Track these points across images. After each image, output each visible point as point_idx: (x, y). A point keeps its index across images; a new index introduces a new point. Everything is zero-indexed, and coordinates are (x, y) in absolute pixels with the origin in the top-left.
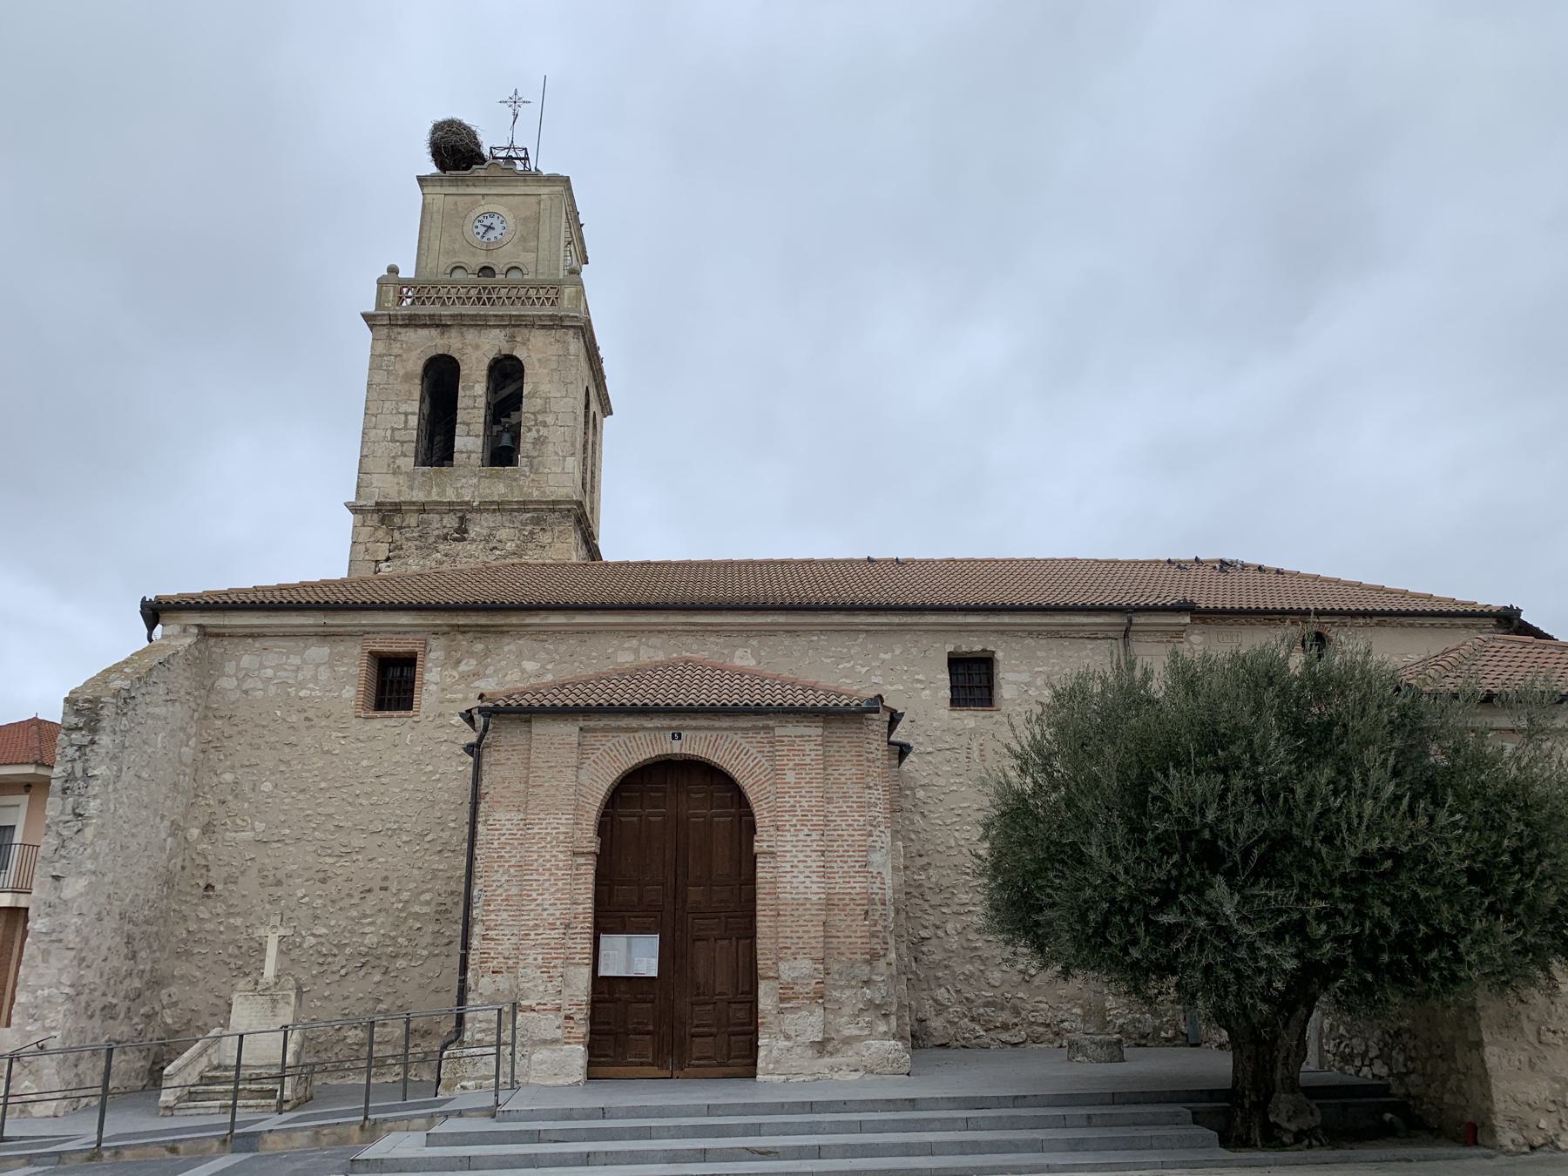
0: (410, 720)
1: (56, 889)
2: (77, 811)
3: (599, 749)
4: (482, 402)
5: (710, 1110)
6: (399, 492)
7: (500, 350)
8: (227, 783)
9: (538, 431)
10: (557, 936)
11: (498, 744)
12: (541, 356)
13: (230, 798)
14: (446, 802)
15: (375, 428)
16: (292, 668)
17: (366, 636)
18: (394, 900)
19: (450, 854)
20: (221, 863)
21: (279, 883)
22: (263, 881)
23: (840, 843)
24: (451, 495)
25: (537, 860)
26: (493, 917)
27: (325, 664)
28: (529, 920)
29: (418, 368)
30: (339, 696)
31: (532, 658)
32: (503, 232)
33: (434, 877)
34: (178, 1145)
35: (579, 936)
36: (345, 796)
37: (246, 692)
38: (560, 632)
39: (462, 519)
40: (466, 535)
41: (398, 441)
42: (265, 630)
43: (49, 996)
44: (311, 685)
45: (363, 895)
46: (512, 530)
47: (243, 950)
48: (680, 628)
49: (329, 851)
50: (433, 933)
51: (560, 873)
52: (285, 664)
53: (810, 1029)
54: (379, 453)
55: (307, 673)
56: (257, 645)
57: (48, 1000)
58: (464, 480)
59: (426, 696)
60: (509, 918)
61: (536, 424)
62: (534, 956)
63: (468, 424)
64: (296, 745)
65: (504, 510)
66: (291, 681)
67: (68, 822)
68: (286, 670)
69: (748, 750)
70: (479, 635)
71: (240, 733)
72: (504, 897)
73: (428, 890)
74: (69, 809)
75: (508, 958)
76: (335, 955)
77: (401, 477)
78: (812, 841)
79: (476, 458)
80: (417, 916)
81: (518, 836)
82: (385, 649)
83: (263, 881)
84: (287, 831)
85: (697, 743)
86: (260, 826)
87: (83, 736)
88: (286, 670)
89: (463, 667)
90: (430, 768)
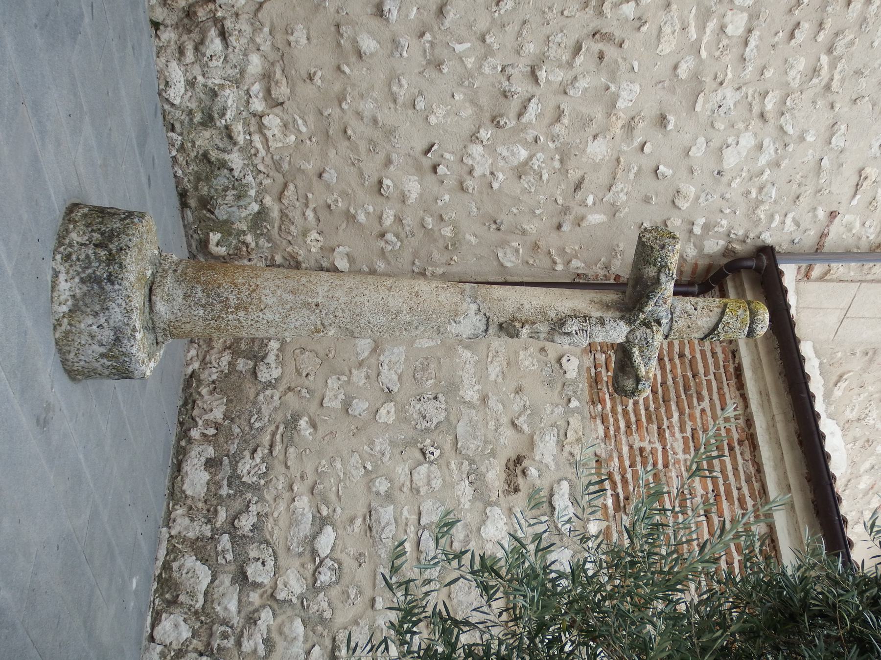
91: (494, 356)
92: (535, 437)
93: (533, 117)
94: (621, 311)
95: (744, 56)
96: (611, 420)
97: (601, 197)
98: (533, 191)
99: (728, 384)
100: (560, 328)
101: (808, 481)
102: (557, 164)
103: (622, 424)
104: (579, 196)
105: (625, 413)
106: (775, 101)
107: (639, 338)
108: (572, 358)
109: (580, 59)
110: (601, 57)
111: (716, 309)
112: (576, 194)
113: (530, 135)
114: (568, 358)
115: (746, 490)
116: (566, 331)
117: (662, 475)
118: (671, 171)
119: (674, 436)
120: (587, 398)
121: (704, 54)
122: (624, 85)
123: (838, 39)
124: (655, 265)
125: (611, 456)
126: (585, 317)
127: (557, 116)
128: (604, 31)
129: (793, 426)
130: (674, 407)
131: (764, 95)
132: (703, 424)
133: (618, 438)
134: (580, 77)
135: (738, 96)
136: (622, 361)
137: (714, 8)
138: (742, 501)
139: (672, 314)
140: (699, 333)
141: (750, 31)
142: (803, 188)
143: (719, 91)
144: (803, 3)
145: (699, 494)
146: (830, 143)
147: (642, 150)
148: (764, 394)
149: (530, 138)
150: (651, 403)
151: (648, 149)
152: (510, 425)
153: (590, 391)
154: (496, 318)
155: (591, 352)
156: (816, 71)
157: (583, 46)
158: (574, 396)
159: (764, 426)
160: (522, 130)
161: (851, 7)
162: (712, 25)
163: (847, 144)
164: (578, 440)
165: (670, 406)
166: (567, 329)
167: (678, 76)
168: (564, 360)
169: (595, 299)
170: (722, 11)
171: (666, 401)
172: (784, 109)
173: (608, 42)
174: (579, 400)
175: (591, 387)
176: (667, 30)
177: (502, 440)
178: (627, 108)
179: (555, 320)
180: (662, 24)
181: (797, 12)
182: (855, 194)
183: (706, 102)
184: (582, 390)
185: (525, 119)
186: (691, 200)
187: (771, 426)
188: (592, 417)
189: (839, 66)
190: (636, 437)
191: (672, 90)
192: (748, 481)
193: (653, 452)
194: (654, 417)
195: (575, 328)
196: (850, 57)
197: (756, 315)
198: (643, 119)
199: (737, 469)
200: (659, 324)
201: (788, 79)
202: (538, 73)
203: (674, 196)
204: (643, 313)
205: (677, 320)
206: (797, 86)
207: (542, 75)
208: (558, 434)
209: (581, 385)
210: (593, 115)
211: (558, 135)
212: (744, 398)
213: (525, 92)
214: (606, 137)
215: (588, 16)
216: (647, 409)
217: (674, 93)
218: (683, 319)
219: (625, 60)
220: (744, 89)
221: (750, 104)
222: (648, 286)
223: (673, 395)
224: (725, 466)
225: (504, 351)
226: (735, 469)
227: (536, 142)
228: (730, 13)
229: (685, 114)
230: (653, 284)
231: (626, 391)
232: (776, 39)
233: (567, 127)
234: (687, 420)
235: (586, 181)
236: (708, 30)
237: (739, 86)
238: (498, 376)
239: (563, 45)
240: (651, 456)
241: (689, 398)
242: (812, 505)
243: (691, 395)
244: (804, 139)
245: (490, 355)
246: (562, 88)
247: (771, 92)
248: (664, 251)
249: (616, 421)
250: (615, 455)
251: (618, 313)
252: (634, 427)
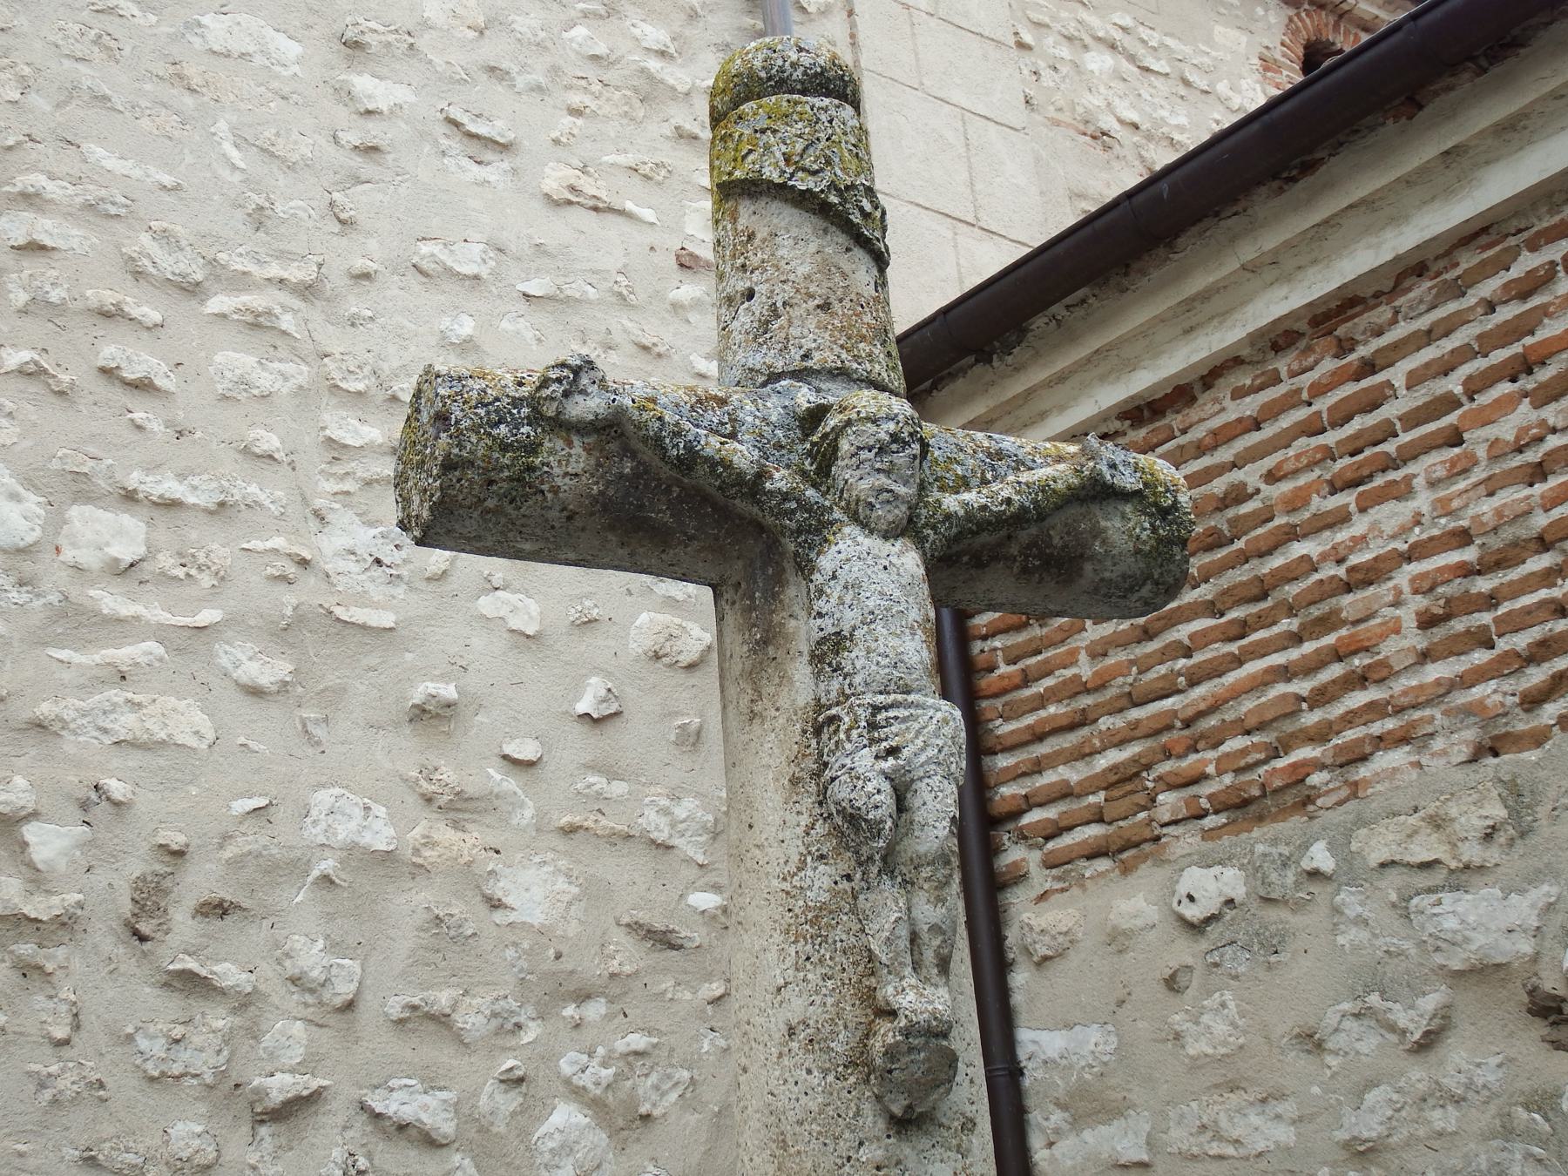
91: (1218, 1137)
92: (1456, 965)
93: (434, 1100)
94: (779, 580)
95: (212, 507)
96: (1350, 735)
97: (695, 871)
98: (686, 1074)
99: (1184, 432)
100: (875, 829)
101: (1420, 107)
102: (595, 1010)
103: (1357, 699)
104: (694, 934)
105: (1321, 697)
106: (356, 422)
107: (883, 480)
108: (1183, 889)
109: (229, 974)
110: (219, 909)
111: (743, 222)
112: (688, 944)
113: (502, 1103)
114: (1185, 901)
115: (1490, 287)
116: (886, 799)
117: (1495, 543)
118: (594, 680)
119: (1364, 537)
120: (1297, 821)
121: (207, 616)
122: (315, 834)
123: (152, 270)
124: (533, 448)
125: (1468, 711)
126: (818, 732)
127: (432, 1027)
128: (127, 908)
129: (1262, 203)
130: (1277, 561)
131: (336, 449)
132: (1310, 467)
133: (1404, 701)
134: (291, 968)
135: (343, 518)
136: (1025, 570)
137: (54, 598)
138: (1525, 289)
139: (774, 377)
140: (847, 267)
141: (130, 497)
142: (618, 337)
143: (329, 567)
144: (36, 363)
145: (1534, 416)
146: (476, 277)
147: (531, 764)
148: (1189, 318)
149: (509, 1102)
150: (1276, 630)
151: (526, 750)
152: (1432, 1057)
153: (1275, 819)
154: (865, 1154)
155: (1157, 839)
156: (257, 324)
157: (177, 966)
158: (1297, 863)
159: (1281, 291)
160: (483, 1131)
161: (48, 242)
162: (111, 601)
163: (474, 235)
164: (1437, 823)
165: (1273, 573)
166: (876, 797)
167: (286, 684)
168: (1193, 913)
169: (744, 701)
170: (63, 575)
171: (1261, 590)
172: (381, 396)
173: (166, 893)
174: (1305, 846)
175: (1260, 819)
176: (126, 724)
177: (1489, 1076)
178: (392, 818)
179: (845, 863)
180: (107, 740)
181: (65, 378)
182: (622, 213)
183: (362, 599)
184: (1274, 842)
185: (445, 1126)
186: (677, 621)
187: (1272, 268)
188: (1354, 795)
189: (239, 267)
190: (1389, 648)
191: (334, 697)
192: (1458, 289)
193: (1427, 586)
194: (1315, 611)
195: (865, 760)
196: (209, 241)
197: (752, 74)
198: (429, 773)
199: (1429, 332)
200: (816, 415)
201: (285, 391)
202: (276, 1098)
203: (670, 666)
204: (762, 475)
205: (796, 354)
206: (305, 368)
207: (281, 1086)
208: (1430, 891)
209: (1260, 848)
210: (421, 917)
211: (495, 1015)
212: (1212, 375)
213: (349, 1134)
214: (491, 873)
215: (77, 964)
216: (1297, 639)
217: (341, 691)
218: (794, 332)
219: (226, 838)
220: (319, 503)
221: (368, 483)
222: (642, 471)
223: (1241, 575)
224: (1427, 365)
225: (1194, 1105)
226: (1428, 337)
227: (520, 1081)
228: (68, 554)
229: (409, 656)
230: (628, 451)
231: (1160, 540)
232: (156, 426)
233: (466, 993)
234: (1307, 515)
235: (643, 917)
236: (126, 609)
237: (311, 517)
238: (1278, 1117)
239: (178, 1031)
240: (1440, 590)
241: (1240, 527)
242: (1496, 70)
243: (1233, 522)
244: (469, 340)
245: (1215, 1149)
246: (333, 1020)
247: (328, 432)
248: (457, 413)
249: (1350, 719)
250: (1461, 698)
251: (791, 591)
252: (1357, 662)
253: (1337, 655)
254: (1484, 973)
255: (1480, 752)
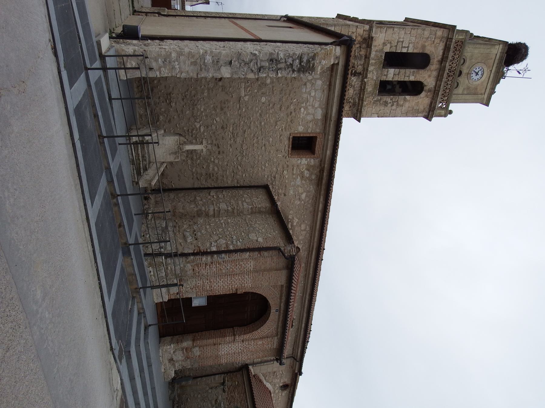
0: (287, 155)
1: (226, 63)
2: (262, 69)
3: (275, 289)
4: (406, 79)
5: (153, 389)
6: (376, 46)
7: (426, 86)
8: (266, 80)
9: (390, 103)
10: (207, 288)
11: (280, 258)
12: (420, 103)
13: (259, 83)
14: (253, 172)
15: (405, 33)
16: (314, 104)
17: (324, 134)
18: (215, 157)
19: (232, 175)
20: (231, 83)
21: (222, 109)
22: (223, 102)
23: (237, 355)
24: (371, 68)
25: (235, 279)
26: (214, 266)
27: (314, 117)
28: (213, 279)
29: (427, 51)
30: (299, 125)
31: (306, 196)
32: (474, 80)
33: (223, 171)
34: (122, 227)
35: (207, 293)
36: (258, 133)
37: (305, 84)
38: (315, 204)
39: (360, 74)
40: (353, 76)
41: (397, 44)
42: (331, 100)
43: (175, 68)
44: (305, 112)
45: (217, 145)
46: (352, 94)
47: (193, 98)
48: (312, 244)
49: (235, 129)
50: (202, 173)
51: (230, 286)
52: (316, 100)
53: (177, 357)
54: (394, 36)
55: (311, 110)
56: (326, 87)
57: (173, 68)
58: (376, 74)
59: (296, 159)
60: (214, 271)
61: (393, 102)
62: (200, 283)
63: (398, 74)
64: (280, 110)
65: (361, 91)
66: (308, 103)
67: (257, 64)
68: (313, 101)
69: (270, 330)
70: (318, 177)
71: (288, 84)
72: (221, 268)
73: (218, 169)
74: (263, 64)
75: (199, 273)
76: (192, 136)
77: (382, 46)
78: (238, 350)
79: (384, 78)
80: (208, 166)
81: (244, 270)
82: (317, 143)
83: (223, 102)
84: (244, 110)
85: (274, 316)
86: (246, 99)
87: (297, 66)
88: (313, 101)
89: (306, 172)
90: (267, 165)
103: (229, 393)
105: (230, 391)
253: (232, 391)
254: (218, 397)
255: (227, 398)
